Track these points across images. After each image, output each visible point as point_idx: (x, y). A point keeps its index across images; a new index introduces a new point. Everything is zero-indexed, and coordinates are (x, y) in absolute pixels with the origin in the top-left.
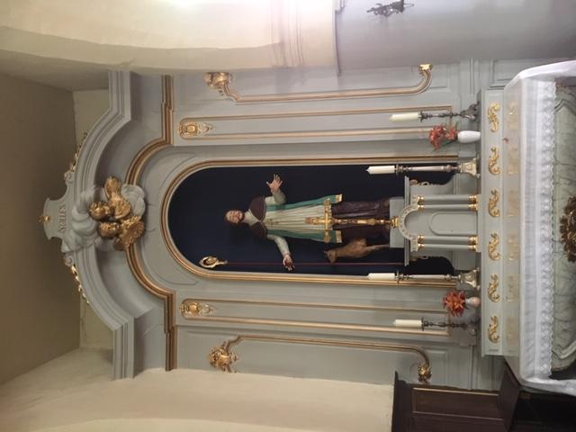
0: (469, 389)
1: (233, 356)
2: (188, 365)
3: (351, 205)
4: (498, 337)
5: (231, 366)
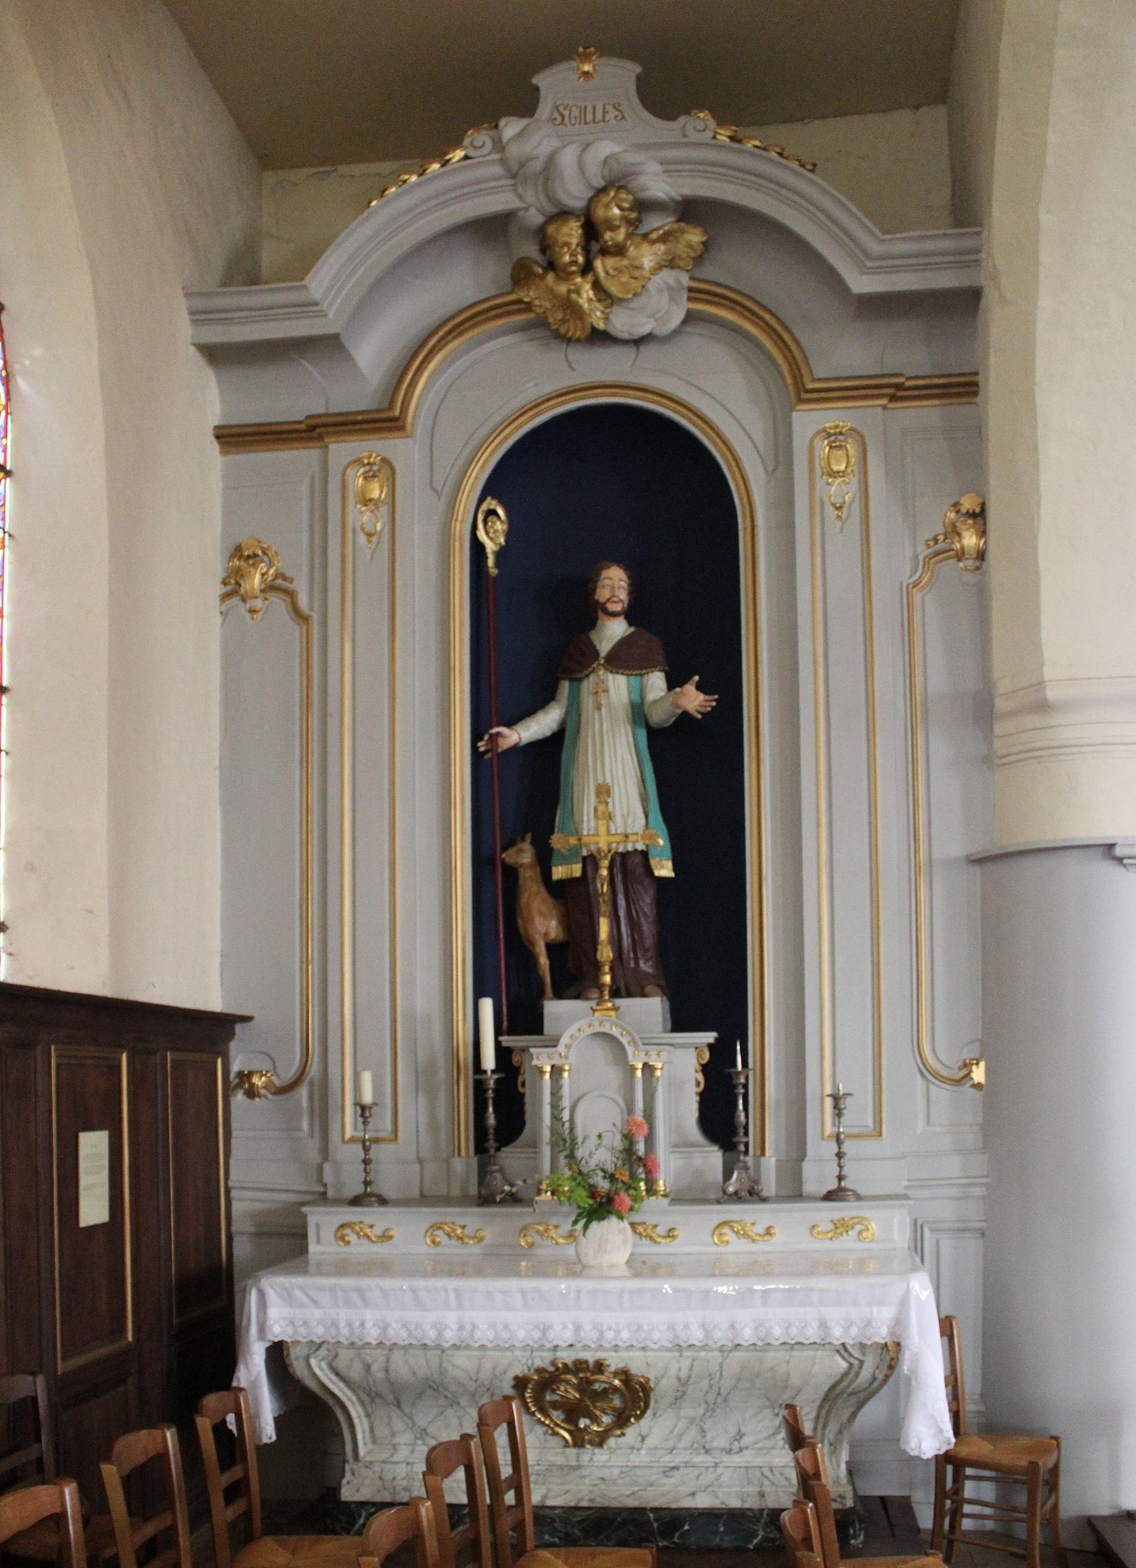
0: (230, 1184)
1: (258, 603)
2: (232, 484)
3: (647, 901)
4: (348, 1243)
5: (235, 601)
